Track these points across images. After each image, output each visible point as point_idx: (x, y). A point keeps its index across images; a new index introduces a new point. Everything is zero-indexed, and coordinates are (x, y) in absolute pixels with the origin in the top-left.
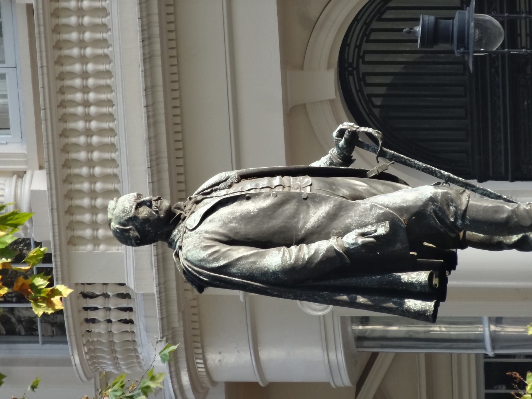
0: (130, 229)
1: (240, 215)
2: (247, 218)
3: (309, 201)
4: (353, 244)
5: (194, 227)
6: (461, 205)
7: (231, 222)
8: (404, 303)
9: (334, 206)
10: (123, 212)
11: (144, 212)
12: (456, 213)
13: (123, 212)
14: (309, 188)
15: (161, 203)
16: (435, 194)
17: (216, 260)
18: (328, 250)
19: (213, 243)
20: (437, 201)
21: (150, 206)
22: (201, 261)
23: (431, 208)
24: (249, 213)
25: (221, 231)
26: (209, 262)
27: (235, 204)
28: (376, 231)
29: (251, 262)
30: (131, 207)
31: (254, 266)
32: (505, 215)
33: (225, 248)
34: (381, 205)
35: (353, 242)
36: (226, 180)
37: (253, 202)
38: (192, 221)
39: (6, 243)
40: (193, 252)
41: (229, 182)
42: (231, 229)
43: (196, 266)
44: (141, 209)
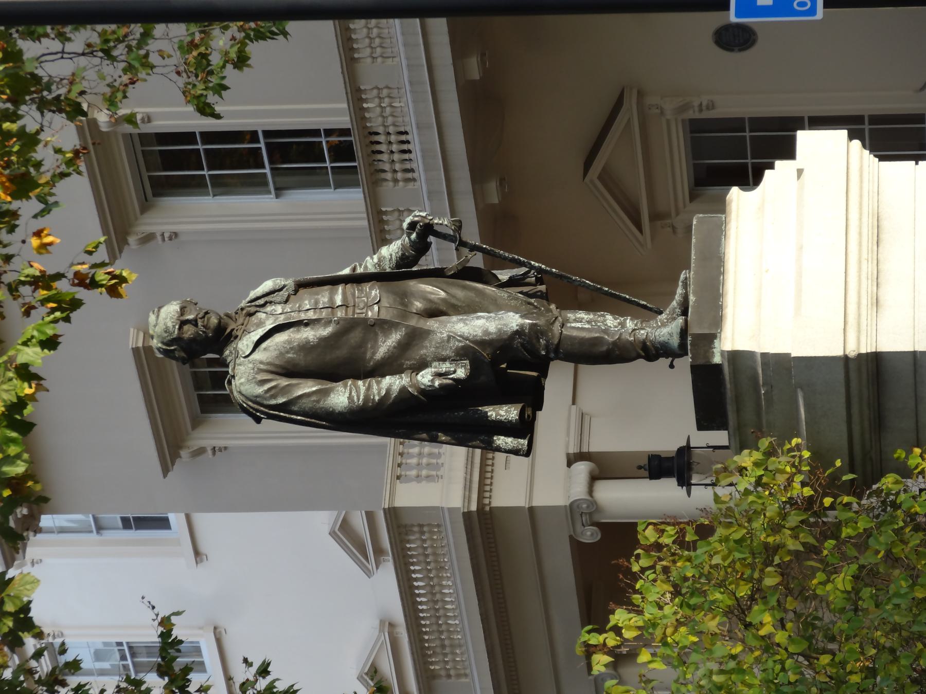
0: (175, 350)
1: (298, 345)
2: (305, 348)
3: (377, 329)
4: (430, 386)
5: (247, 353)
6: (553, 337)
7: (288, 352)
8: (493, 441)
9: (406, 334)
10: (166, 332)
11: (189, 331)
12: (547, 347)
13: (166, 332)
14: (376, 308)
15: (209, 319)
16: (522, 326)
17: (274, 397)
18: (403, 390)
19: (269, 377)
20: (525, 335)
21: (196, 325)
22: (257, 397)
23: (518, 341)
24: (308, 342)
25: (277, 362)
26: (266, 399)
27: (291, 330)
28: (455, 372)
29: (314, 401)
30: (174, 326)
31: (318, 406)
32: (605, 348)
33: (284, 382)
34: (460, 336)
35: (430, 384)
36: (280, 290)
37: (312, 329)
38: (245, 344)
39: (46, 334)
40: (247, 387)
41: (284, 294)
42: (289, 361)
43: (251, 401)
44: (186, 327)
